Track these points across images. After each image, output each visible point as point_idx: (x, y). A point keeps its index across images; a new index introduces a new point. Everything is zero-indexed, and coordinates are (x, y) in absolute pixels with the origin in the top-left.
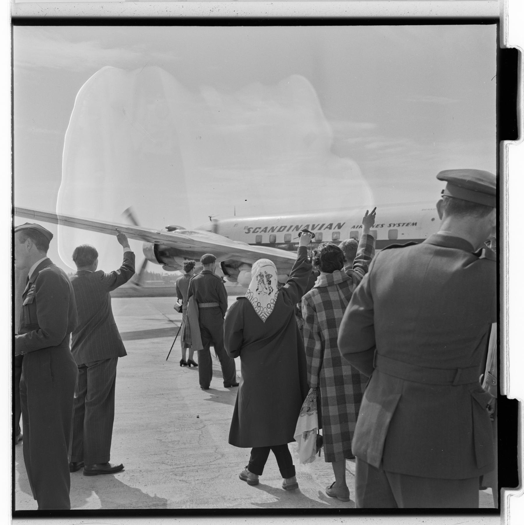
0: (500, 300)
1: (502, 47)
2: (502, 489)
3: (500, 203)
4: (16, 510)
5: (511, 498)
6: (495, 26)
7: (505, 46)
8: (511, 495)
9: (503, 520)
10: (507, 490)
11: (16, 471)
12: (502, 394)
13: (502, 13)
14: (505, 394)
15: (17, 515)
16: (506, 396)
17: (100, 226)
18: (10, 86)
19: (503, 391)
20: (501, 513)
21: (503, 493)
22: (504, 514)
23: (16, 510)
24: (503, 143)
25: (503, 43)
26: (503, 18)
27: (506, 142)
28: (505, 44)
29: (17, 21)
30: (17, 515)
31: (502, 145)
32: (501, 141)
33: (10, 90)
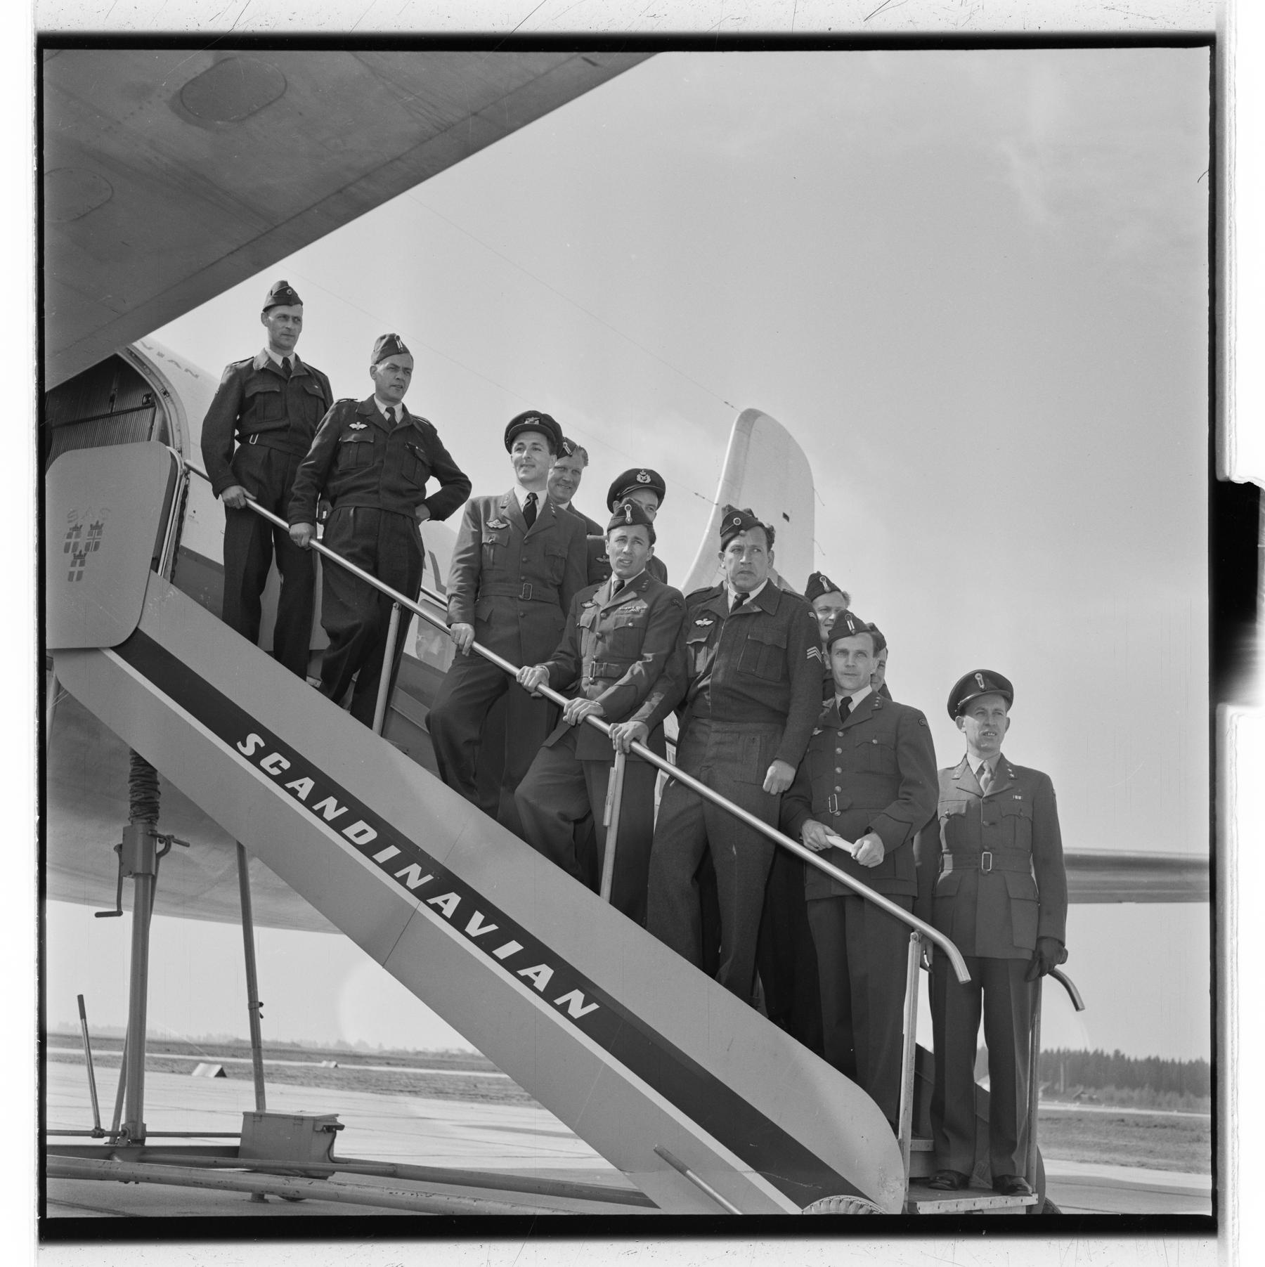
6: (1206, 50)
9: (1223, 1247)
13: (1221, 24)
22: (1224, 1238)
26: (1223, 38)
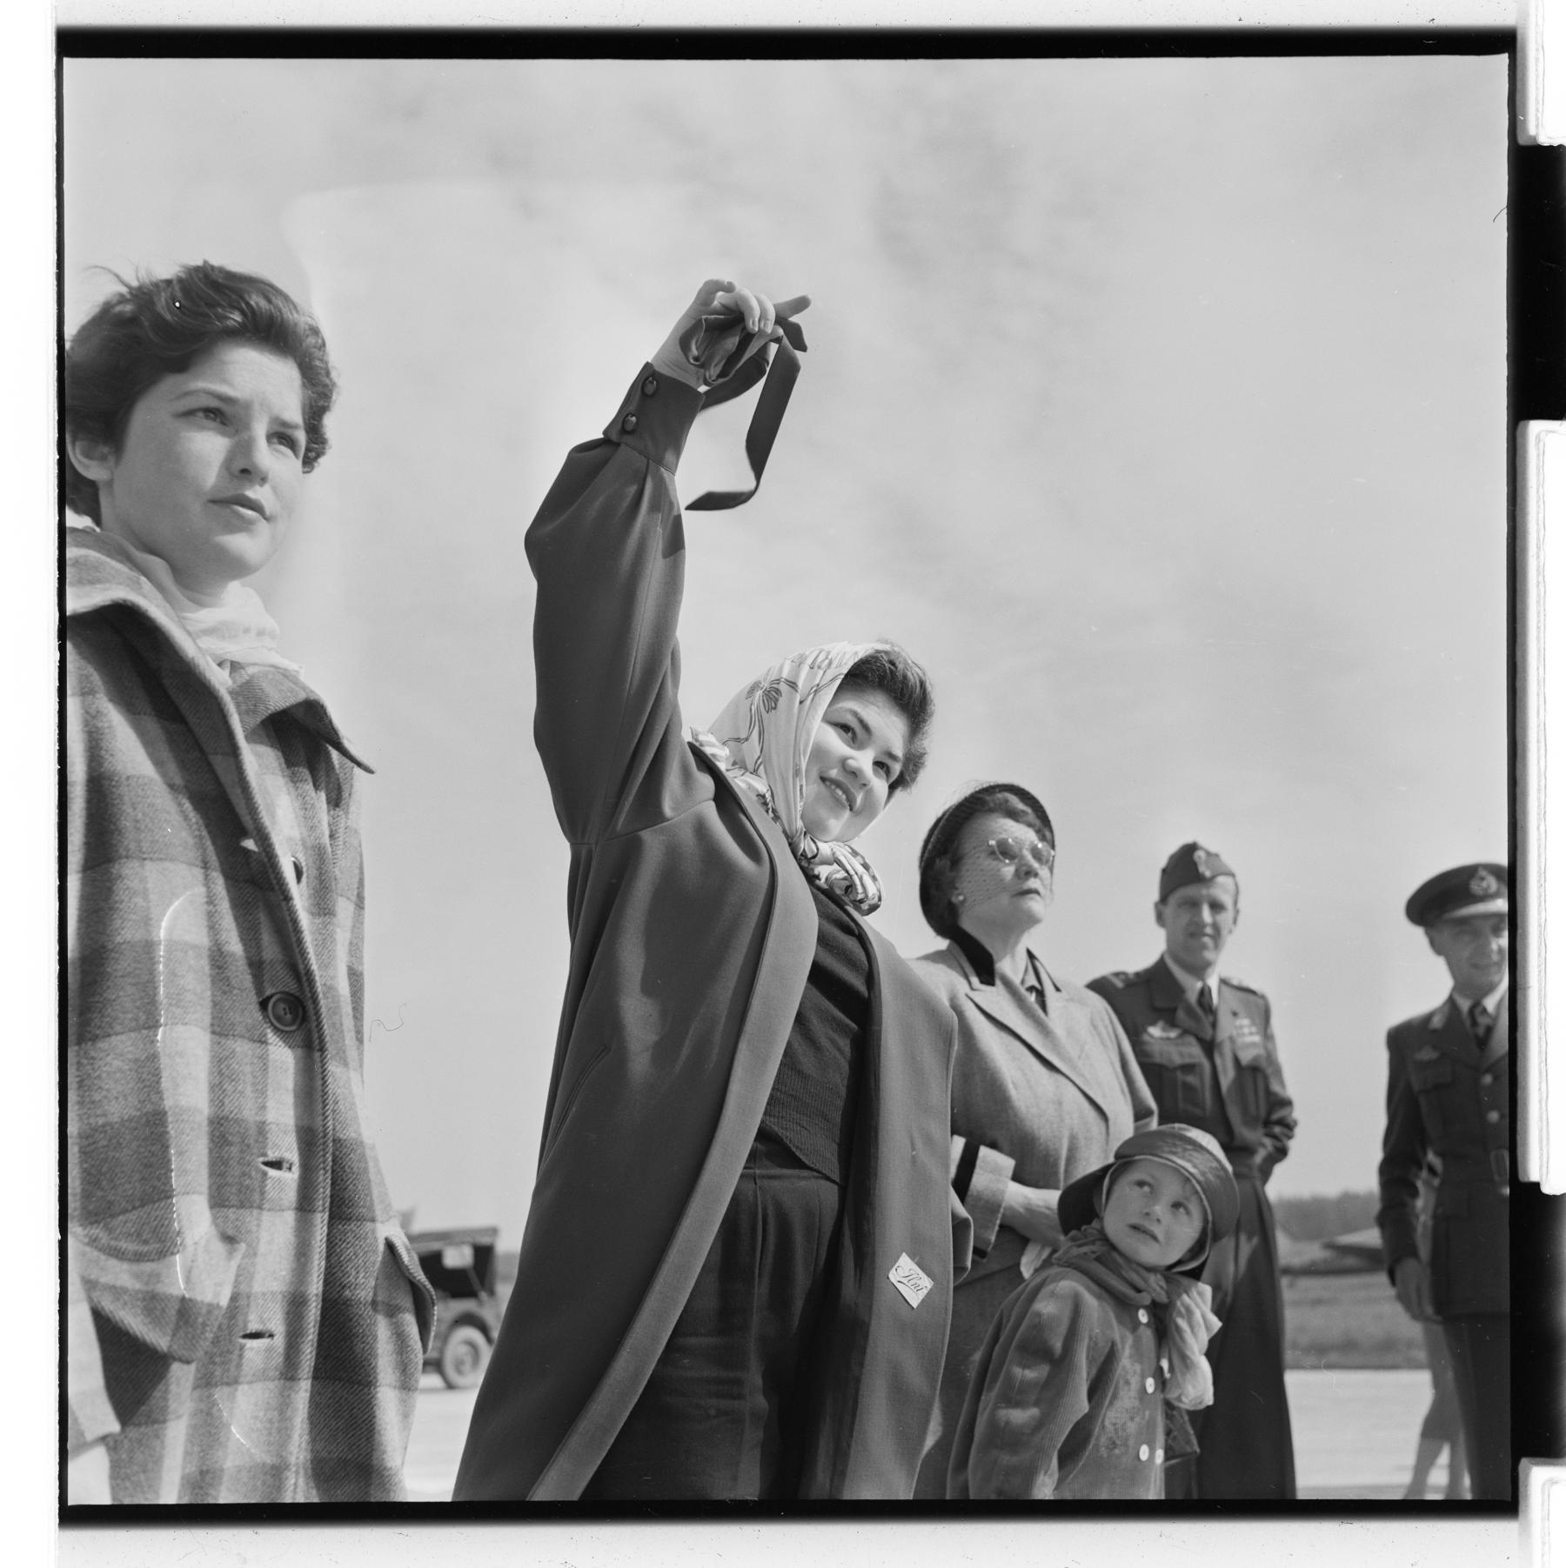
0: (1520, 1159)
1: (1522, 141)
2: (1524, 1462)
3: (1519, 1109)
4: (70, 1503)
5: (1555, 1489)
7: (1535, 138)
8: (1553, 1482)
9: (1526, 1532)
10: (1537, 1464)
11: (71, 1115)
12: (1522, 1178)
13: (1524, 14)
14: (1534, 1176)
15: (73, 1516)
16: (1537, 1185)
17: (320, 1221)
18: (54, 747)
19: (1526, 1171)
20: (1521, 1508)
21: (1527, 1475)
23: (70, 1503)
24: (1526, 427)
25: (1525, 129)
27: (1536, 429)
28: (1532, 131)
29: (76, 43)
30: (73, 1516)
31: (1524, 435)
32: (1522, 424)
33: (53, 269)
